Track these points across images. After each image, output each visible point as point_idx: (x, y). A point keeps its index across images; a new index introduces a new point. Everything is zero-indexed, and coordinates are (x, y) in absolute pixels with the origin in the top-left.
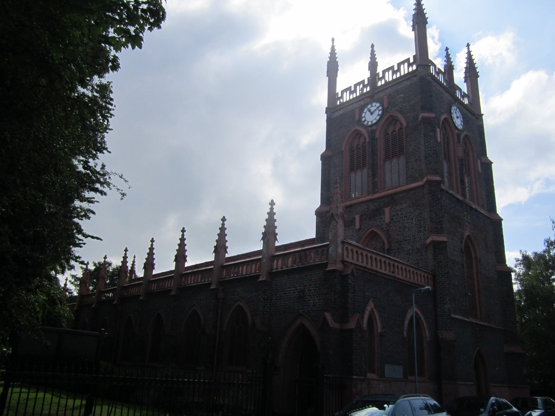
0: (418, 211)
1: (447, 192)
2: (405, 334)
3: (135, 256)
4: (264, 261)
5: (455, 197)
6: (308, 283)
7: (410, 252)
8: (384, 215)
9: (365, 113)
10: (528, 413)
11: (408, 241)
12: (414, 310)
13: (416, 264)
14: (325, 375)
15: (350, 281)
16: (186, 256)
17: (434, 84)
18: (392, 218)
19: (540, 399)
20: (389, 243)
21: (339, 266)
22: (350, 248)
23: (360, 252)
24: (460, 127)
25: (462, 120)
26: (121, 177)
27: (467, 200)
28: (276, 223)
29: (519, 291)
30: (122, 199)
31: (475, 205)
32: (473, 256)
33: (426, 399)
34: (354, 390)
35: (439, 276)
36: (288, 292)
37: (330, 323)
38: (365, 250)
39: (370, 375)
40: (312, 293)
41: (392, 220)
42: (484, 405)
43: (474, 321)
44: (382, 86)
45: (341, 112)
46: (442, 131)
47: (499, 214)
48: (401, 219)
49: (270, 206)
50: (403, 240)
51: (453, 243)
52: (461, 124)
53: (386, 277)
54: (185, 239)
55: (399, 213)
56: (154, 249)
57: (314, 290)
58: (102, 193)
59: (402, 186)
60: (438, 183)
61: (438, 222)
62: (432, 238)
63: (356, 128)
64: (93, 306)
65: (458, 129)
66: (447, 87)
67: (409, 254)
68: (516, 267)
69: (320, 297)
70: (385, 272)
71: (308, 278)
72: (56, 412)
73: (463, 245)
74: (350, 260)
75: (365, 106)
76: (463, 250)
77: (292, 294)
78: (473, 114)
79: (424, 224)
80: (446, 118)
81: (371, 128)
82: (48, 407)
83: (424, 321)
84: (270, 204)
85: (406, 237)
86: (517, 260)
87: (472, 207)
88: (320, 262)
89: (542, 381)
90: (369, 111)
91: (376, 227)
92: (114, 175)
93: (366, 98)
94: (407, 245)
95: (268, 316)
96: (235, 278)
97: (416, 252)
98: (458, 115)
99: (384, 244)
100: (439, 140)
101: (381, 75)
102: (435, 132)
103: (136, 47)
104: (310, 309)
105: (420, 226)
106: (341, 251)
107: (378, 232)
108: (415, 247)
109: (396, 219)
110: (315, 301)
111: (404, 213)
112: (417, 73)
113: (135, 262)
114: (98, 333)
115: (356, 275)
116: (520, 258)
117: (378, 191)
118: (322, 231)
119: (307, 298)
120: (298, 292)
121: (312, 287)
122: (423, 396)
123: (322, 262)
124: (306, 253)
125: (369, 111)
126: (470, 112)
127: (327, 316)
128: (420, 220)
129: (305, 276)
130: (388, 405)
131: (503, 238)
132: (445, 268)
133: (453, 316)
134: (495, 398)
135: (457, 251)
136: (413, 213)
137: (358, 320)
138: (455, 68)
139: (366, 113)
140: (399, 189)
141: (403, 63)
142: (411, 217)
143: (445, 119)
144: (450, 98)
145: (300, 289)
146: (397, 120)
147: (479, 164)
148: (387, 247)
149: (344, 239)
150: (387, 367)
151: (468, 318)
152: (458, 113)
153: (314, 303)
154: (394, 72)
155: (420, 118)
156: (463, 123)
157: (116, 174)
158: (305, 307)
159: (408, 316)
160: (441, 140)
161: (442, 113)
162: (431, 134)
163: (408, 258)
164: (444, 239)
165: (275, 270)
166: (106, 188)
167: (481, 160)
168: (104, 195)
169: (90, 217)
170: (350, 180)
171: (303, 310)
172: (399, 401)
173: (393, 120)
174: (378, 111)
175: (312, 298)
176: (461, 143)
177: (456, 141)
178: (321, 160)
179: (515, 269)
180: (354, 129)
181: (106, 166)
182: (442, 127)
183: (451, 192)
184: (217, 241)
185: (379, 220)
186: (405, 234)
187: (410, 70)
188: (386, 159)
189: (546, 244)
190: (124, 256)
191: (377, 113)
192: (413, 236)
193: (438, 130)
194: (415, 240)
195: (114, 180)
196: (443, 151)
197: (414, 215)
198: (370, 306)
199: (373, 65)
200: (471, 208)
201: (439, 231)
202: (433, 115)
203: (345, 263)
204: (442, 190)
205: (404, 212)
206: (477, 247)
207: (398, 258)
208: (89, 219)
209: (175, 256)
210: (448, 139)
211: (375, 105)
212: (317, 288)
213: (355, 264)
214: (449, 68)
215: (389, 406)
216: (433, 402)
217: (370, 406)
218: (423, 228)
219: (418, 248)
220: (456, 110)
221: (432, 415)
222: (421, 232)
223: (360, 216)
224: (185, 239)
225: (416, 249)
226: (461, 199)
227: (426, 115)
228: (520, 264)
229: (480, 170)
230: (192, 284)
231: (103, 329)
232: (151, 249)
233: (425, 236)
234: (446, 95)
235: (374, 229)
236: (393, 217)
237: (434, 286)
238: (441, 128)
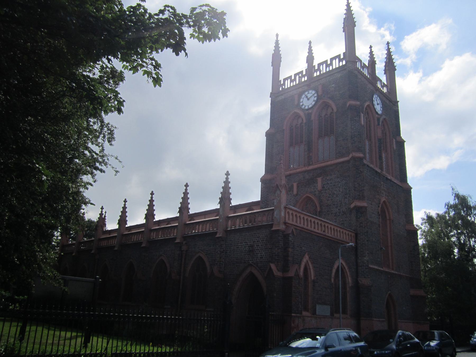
0: (345, 181)
1: (368, 166)
2: (333, 280)
3: (106, 211)
4: (221, 221)
5: (374, 170)
6: (257, 239)
7: (337, 214)
9: (303, 99)
10: (427, 343)
11: (336, 205)
12: (340, 262)
13: (342, 224)
14: (270, 313)
15: (290, 239)
16: (155, 215)
18: (324, 186)
19: (437, 332)
20: (320, 207)
21: (282, 227)
22: (291, 212)
23: (298, 215)
24: (380, 112)
25: (381, 106)
26: (116, 158)
27: (384, 173)
28: (230, 190)
29: (423, 244)
30: (116, 175)
31: (390, 176)
32: (388, 218)
33: (349, 332)
34: (293, 325)
35: (360, 234)
36: (240, 247)
37: (274, 272)
38: (302, 213)
39: (304, 313)
40: (260, 247)
41: (323, 188)
42: (393, 337)
43: (386, 270)
44: (317, 76)
45: (283, 97)
46: (365, 116)
47: (409, 184)
48: (331, 187)
49: (226, 176)
50: (332, 205)
51: (372, 207)
52: (381, 110)
53: (318, 235)
54: (154, 201)
55: (329, 182)
56: (126, 208)
57: (261, 245)
58: (102, 171)
59: (332, 160)
60: (361, 159)
61: (361, 191)
62: (355, 204)
63: (296, 111)
64: (74, 254)
65: (377, 113)
66: (371, 79)
67: (336, 216)
68: (422, 225)
69: (266, 251)
70: (317, 231)
71: (257, 235)
72: (58, 342)
73: (380, 208)
74: (290, 222)
75: (303, 92)
76: (380, 213)
77: (243, 248)
78: (390, 101)
79: (349, 192)
80: (369, 104)
81: (307, 111)
82: (46, 337)
83: (347, 271)
84: (226, 174)
85: (334, 202)
86: (423, 220)
87: (388, 178)
88: (267, 223)
89: (440, 318)
90: (307, 97)
91: (310, 193)
92: (111, 156)
93: (303, 86)
94: (335, 209)
95: (223, 265)
96: (196, 234)
97: (342, 214)
98: (379, 102)
99: (316, 207)
100: (363, 123)
101: (316, 68)
103: (157, 85)
104: (258, 261)
105: (346, 194)
106: (284, 214)
107: (312, 197)
108: (341, 210)
109: (327, 187)
110: (262, 254)
111: (333, 182)
112: (346, 67)
113: (106, 217)
114: (94, 279)
115: (295, 235)
116: (425, 218)
117: (312, 164)
118: (266, 195)
119: (255, 252)
120: (249, 246)
121: (260, 243)
122: (347, 330)
123: (269, 223)
124: (255, 216)
125: (307, 97)
126: (388, 99)
127: (272, 266)
128: (346, 189)
129: (254, 234)
130: (320, 336)
131: (412, 203)
132: (365, 228)
133: (371, 266)
134: (401, 331)
136: (340, 183)
137: (297, 269)
139: (303, 98)
140: (329, 163)
141: (335, 58)
142: (339, 186)
143: (368, 106)
144: (372, 88)
145: (250, 244)
147: (394, 143)
148: (318, 209)
149: (287, 205)
150: (318, 307)
151: (382, 268)
152: (378, 101)
153: (261, 255)
154: (292, 81)
155: (348, 105)
156: (382, 109)
157: (113, 156)
158: (254, 259)
159: (335, 267)
160: (364, 123)
162: (356, 118)
163: (336, 219)
164: (365, 204)
165: (230, 228)
166: (103, 166)
167: (396, 139)
168: (103, 173)
169: (88, 188)
170: (290, 154)
171: (252, 261)
172: (329, 333)
173: (326, 106)
174: (313, 97)
175: (259, 251)
176: (380, 126)
178: (265, 136)
179: (421, 226)
180: (293, 111)
181: (105, 150)
182: (365, 113)
183: (371, 166)
184: (181, 203)
185: (313, 187)
186: (334, 200)
187: (341, 64)
189: (447, 207)
190: (100, 213)
192: (340, 201)
193: (362, 115)
194: (341, 204)
195: (112, 161)
196: (366, 132)
197: (341, 184)
198: (306, 258)
199: (310, 59)
200: (387, 179)
201: (361, 198)
202: (358, 103)
203: (287, 224)
204: (364, 165)
205: (333, 182)
206: (390, 211)
207: (327, 219)
208: (87, 190)
209: (145, 215)
210: (370, 122)
211: (311, 93)
212: (264, 244)
213: (294, 225)
214: (372, 62)
215: (320, 338)
216: (354, 334)
217: (306, 338)
218: (348, 195)
219: (344, 211)
220: (377, 98)
221: (353, 344)
222: (346, 199)
223: (298, 184)
224: (154, 201)
225: (342, 212)
226: (379, 172)
227: (353, 102)
228: (425, 223)
229: (395, 148)
230: (160, 238)
231: (97, 277)
232: (124, 208)
233: (350, 202)
235: (308, 195)
236: (325, 185)
237: (356, 243)
238: (364, 113)
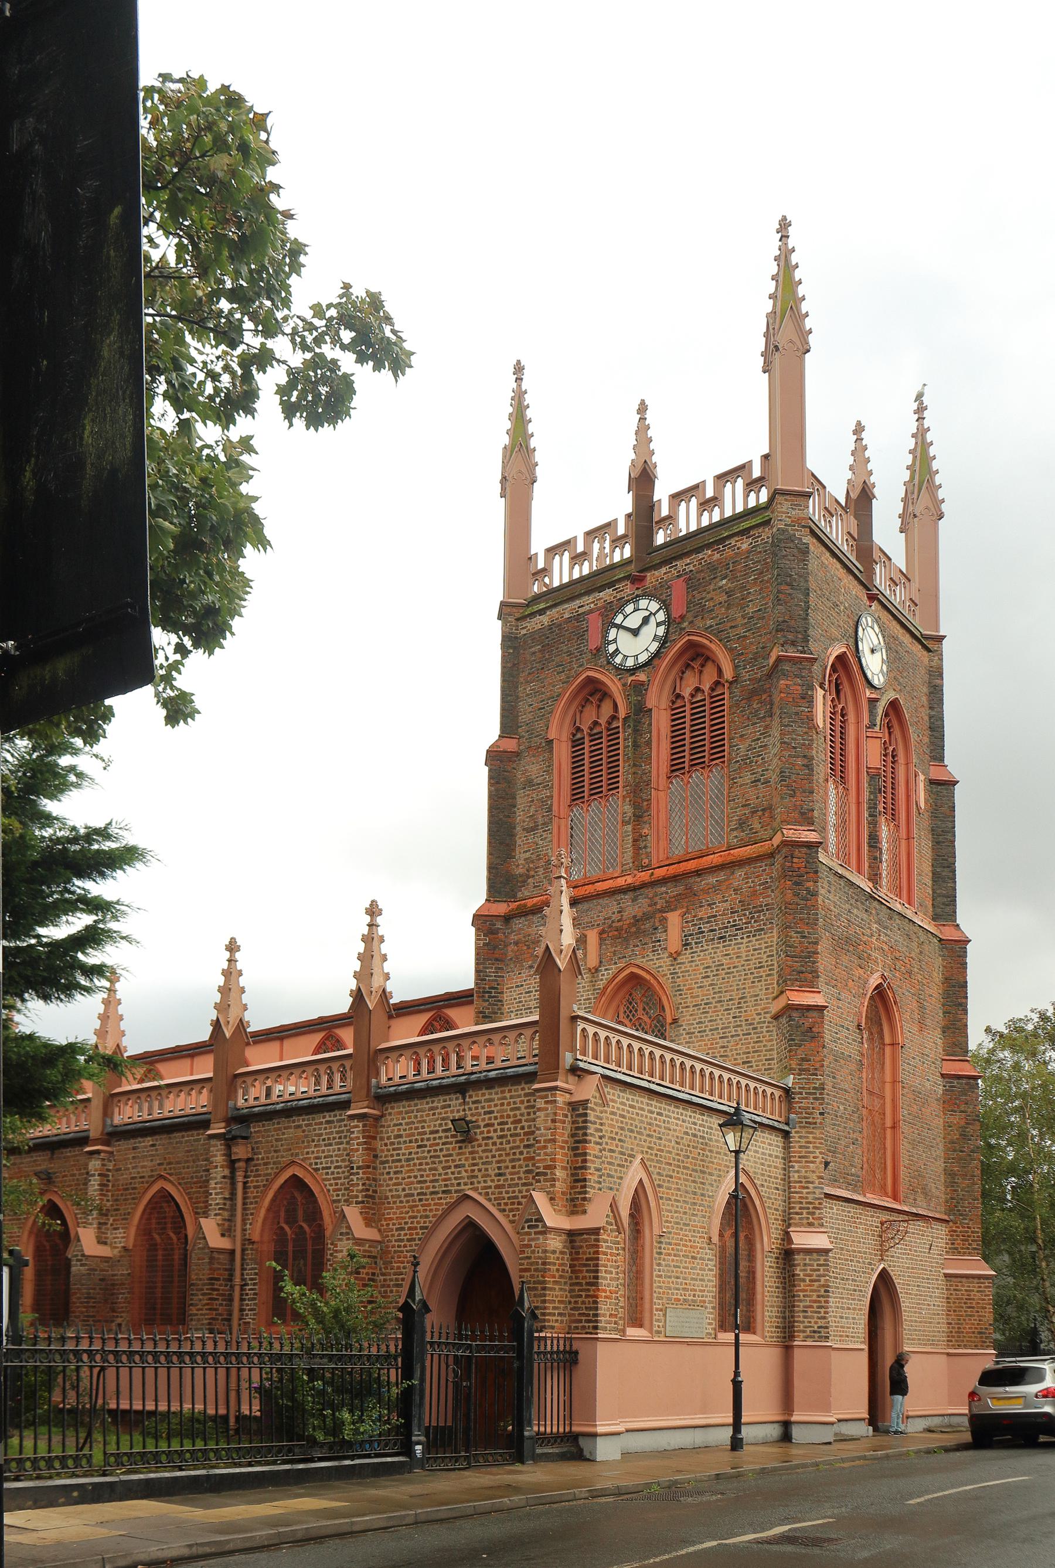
8: (666, 931)
14: (536, 1335)
17: (815, 547)
25: (885, 657)
55: (705, 928)
60: (812, 847)
65: (871, 686)
102: (810, 701)
135: (848, 1029)
136: (742, 929)
138: (876, 494)
143: (841, 659)
146: (708, 659)
154: (706, 505)
161: (833, 640)
177: (866, 721)
188: (673, 771)
191: (650, 631)
210: (843, 716)
234: (848, 581)
